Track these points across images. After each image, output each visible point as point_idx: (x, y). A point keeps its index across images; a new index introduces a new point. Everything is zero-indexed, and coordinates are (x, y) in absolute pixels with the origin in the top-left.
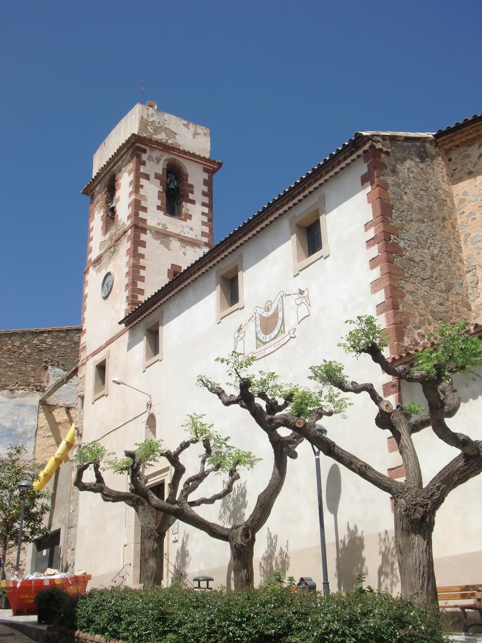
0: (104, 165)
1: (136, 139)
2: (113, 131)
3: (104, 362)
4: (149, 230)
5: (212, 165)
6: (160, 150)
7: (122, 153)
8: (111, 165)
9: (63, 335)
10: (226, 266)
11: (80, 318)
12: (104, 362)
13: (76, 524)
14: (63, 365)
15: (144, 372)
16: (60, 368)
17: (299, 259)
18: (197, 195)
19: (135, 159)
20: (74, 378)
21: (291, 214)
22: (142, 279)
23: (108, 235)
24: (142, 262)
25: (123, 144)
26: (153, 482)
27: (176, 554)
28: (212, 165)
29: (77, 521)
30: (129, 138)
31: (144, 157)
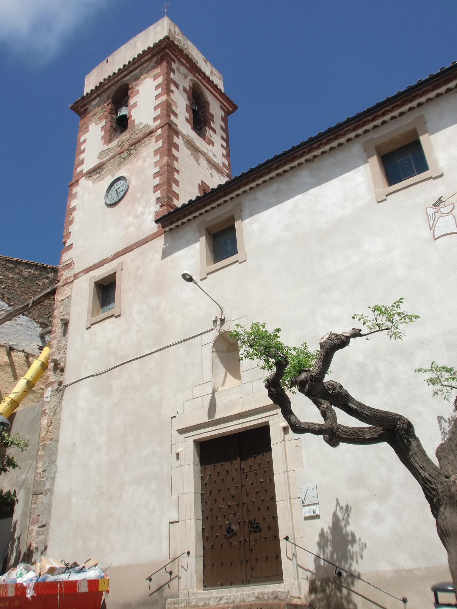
0: (114, 73)
1: (168, 43)
3: (114, 275)
4: (182, 136)
5: (228, 106)
6: (186, 67)
7: (143, 60)
8: (123, 74)
9: (11, 266)
10: (391, 130)
11: (62, 232)
12: (114, 275)
13: (51, 490)
14: (8, 299)
15: (87, 329)
16: (5, 302)
18: (217, 124)
19: (165, 64)
20: (19, 316)
21: (369, 136)
22: (177, 183)
23: (115, 143)
24: (176, 165)
25: (149, 48)
26: (239, 427)
27: (317, 539)
28: (228, 106)
29: (52, 485)
30: (160, 41)
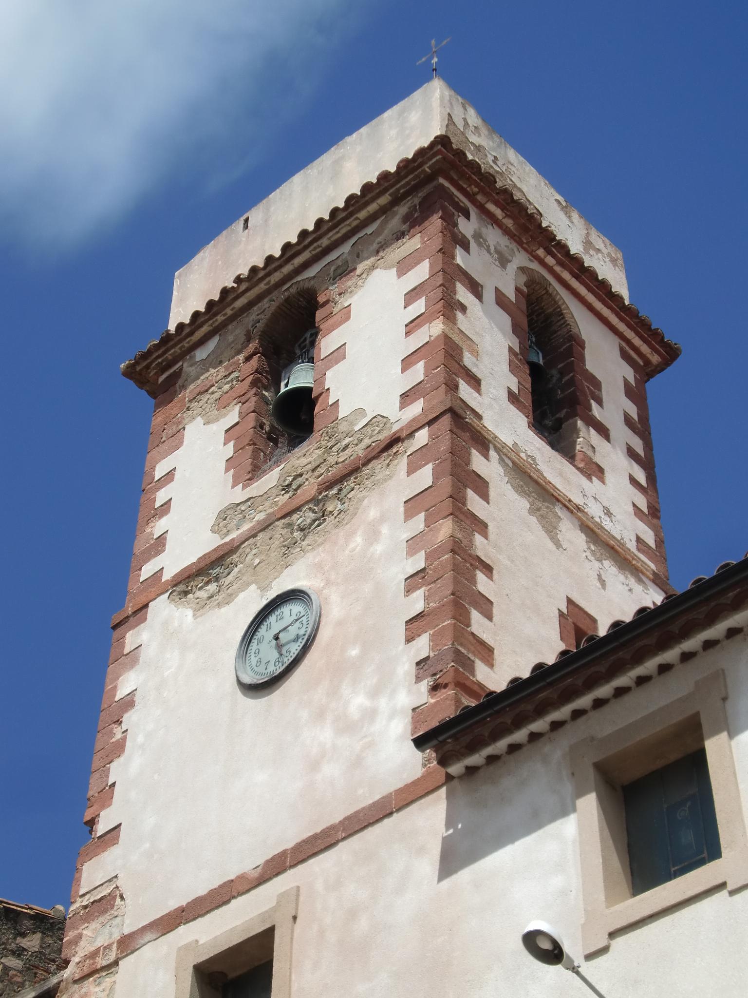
1: (444, 158)
2: (297, 180)
4: (497, 450)
6: (506, 231)
7: (363, 215)
8: (298, 261)
17: (611, 899)
18: (613, 407)
19: (435, 222)
22: (486, 606)
24: (480, 546)
25: (385, 176)
31: (466, 227)
